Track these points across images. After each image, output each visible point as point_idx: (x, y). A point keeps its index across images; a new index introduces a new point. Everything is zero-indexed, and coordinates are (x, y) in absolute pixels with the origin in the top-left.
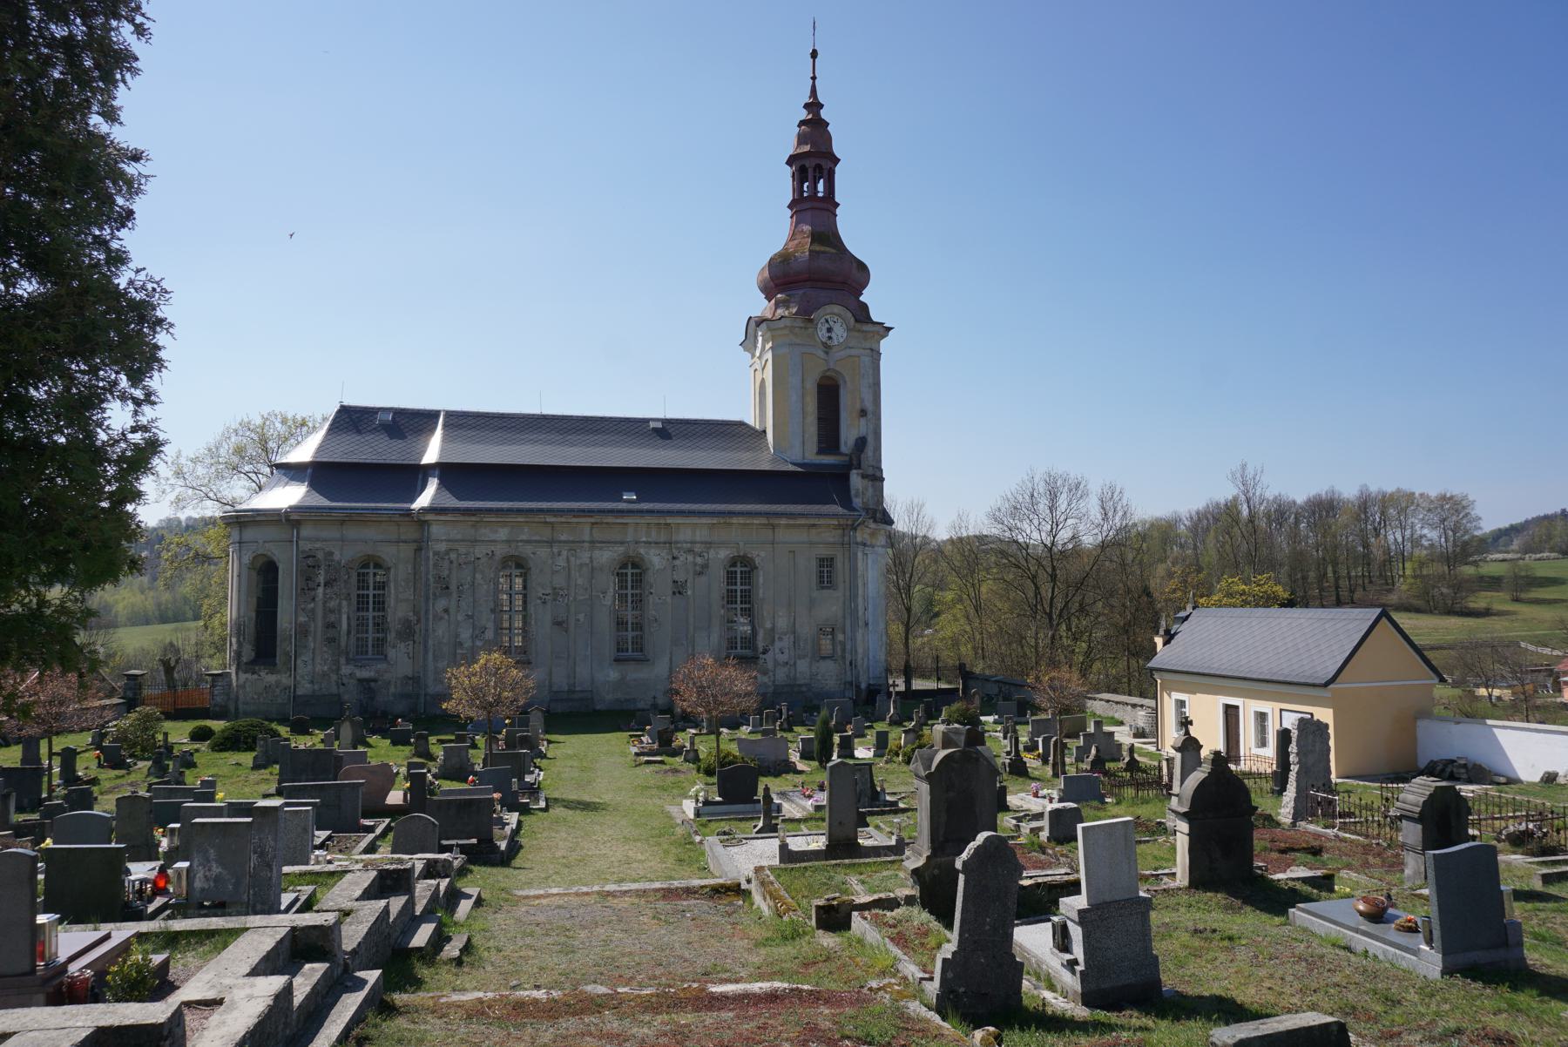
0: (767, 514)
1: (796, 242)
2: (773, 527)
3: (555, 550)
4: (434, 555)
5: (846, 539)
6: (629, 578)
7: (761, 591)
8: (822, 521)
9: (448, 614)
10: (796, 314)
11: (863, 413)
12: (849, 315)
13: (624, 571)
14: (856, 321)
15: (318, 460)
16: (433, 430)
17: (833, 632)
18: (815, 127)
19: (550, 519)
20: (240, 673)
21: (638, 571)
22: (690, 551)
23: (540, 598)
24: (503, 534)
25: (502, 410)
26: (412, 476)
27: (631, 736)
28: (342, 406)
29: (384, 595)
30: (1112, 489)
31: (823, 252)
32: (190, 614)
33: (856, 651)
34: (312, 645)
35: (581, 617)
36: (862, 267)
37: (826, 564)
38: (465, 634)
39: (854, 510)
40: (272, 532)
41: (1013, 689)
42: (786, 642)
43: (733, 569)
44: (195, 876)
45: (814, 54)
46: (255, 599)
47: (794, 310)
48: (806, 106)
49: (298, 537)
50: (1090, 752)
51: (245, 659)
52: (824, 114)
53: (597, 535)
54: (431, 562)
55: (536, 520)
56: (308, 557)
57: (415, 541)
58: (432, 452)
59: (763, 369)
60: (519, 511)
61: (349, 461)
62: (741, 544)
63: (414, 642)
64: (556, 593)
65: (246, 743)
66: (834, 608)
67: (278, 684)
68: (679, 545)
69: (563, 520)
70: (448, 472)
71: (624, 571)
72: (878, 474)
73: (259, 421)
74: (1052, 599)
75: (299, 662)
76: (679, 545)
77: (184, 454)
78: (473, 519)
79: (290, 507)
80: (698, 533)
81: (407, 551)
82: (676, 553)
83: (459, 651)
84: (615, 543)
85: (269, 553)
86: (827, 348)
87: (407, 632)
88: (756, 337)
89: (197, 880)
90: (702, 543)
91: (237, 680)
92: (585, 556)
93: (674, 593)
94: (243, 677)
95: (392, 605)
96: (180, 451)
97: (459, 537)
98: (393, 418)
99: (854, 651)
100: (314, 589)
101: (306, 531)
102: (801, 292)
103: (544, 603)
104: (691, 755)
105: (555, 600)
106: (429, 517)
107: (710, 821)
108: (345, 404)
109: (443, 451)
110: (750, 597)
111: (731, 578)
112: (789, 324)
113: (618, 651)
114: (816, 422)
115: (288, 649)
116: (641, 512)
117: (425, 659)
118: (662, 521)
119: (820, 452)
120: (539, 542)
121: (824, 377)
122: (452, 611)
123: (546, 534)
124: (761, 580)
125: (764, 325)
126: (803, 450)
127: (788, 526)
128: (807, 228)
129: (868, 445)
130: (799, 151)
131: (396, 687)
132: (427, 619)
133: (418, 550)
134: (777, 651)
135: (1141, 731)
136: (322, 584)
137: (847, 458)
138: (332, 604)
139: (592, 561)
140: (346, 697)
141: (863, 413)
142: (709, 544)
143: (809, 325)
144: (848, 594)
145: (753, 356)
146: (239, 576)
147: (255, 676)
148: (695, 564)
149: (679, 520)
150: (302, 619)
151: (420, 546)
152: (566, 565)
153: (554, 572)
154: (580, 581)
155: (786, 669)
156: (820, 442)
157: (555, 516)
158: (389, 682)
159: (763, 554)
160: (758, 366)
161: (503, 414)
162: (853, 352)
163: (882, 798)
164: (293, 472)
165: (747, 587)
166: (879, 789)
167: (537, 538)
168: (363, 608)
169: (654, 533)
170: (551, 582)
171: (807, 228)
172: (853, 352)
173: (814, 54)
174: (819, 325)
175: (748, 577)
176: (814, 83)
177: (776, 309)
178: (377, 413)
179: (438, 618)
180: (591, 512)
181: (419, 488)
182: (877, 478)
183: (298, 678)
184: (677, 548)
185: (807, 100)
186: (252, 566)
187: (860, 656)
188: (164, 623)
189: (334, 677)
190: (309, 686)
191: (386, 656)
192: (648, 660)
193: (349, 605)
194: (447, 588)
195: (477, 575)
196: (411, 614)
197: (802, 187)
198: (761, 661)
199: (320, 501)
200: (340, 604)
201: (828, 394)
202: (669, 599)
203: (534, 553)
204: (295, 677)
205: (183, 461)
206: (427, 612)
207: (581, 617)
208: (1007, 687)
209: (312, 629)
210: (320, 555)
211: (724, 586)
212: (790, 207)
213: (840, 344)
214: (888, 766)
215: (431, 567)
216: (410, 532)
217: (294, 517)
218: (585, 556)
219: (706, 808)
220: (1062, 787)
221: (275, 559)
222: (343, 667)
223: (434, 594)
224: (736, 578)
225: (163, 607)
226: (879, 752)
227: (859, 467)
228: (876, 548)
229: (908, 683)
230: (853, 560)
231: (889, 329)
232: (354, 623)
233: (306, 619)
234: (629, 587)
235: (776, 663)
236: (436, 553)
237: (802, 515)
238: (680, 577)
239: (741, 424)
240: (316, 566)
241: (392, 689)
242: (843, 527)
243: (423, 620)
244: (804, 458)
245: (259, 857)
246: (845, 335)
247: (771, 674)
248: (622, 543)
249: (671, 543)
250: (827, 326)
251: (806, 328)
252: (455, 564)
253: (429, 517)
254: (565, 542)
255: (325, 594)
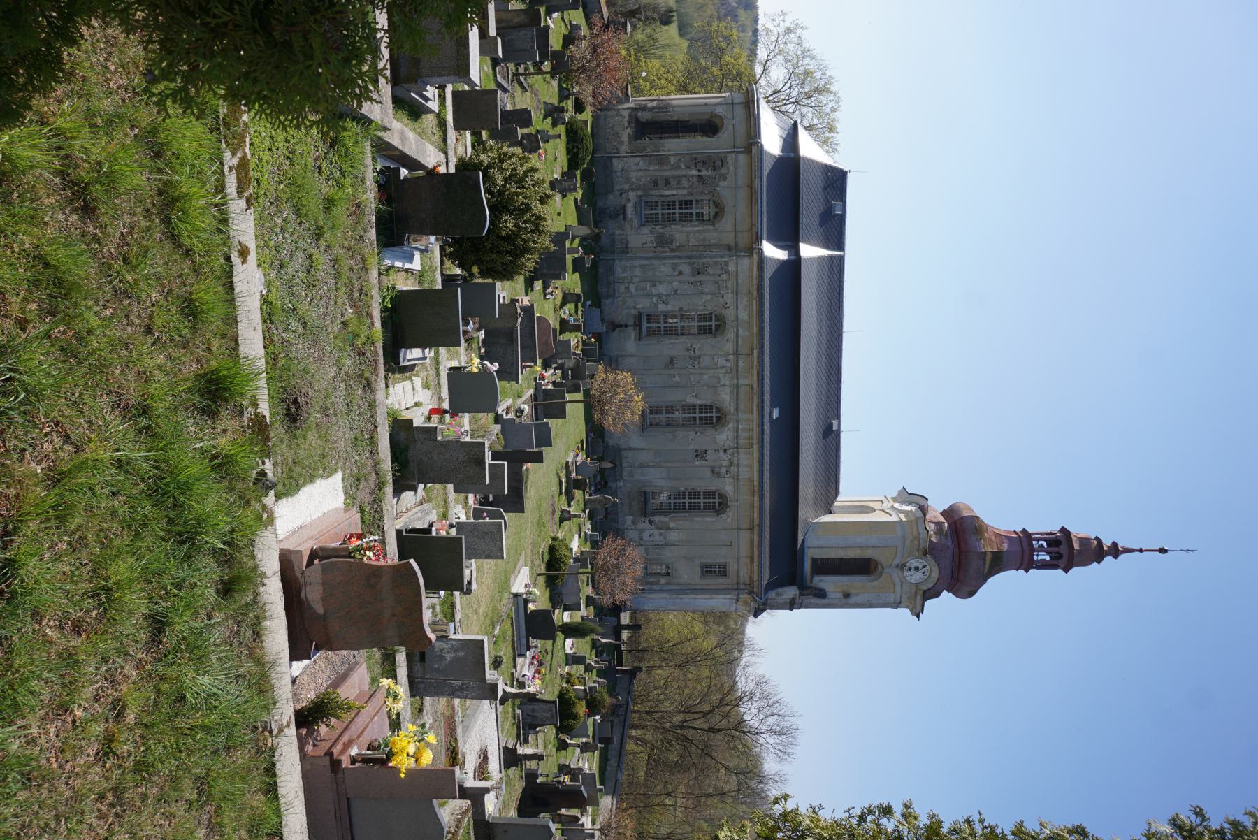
0: (761, 525)
1: (993, 538)
2: (751, 529)
4: (725, 262)
5: (742, 586)
7: (699, 519)
8: (756, 568)
9: (678, 275)
10: (931, 541)
11: (847, 596)
14: (925, 591)
15: (801, 161)
16: (827, 247)
17: (668, 574)
18: (1095, 552)
19: (756, 353)
20: (629, 111)
21: (714, 421)
22: (731, 463)
23: (691, 347)
24: (743, 315)
26: (789, 237)
29: (692, 220)
34: (652, 168)
35: (677, 379)
36: (972, 593)
37: (722, 571)
38: (662, 289)
39: (766, 592)
40: (741, 130)
42: (658, 539)
45: (1163, 551)
46: (688, 119)
47: (934, 539)
48: (1115, 545)
49: (738, 152)
53: (742, 390)
54: (719, 259)
55: (755, 342)
56: (722, 161)
57: (736, 245)
58: (808, 251)
59: (883, 511)
60: (762, 329)
61: (801, 186)
62: (737, 504)
63: (655, 247)
64: (696, 358)
65: (573, 148)
66: (686, 576)
67: (621, 143)
68: (736, 455)
69: (755, 363)
70: (793, 266)
72: (796, 606)
73: (833, 89)
74: (695, 729)
75: (638, 159)
76: (736, 455)
78: (755, 292)
79: (762, 146)
80: (746, 469)
81: (728, 239)
82: (730, 452)
83: (648, 285)
84: (737, 404)
85: (724, 129)
86: (902, 567)
87: (663, 242)
88: (910, 503)
89: (441, 643)
90: (738, 472)
92: (726, 380)
93: (697, 451)
94: (626, 114)
95: (684, 229)
96: (806, 29)
98: (838, 215)
101: (742, 159)
102: (950, 544)
103: (688, 350)
104: (566, 515)
105: (690, 358)
106: (756, 257)
107: (512, 618)
109: (811, 260)
110: (695, 509)
111: (710, 495)
112: (922, 536)
113: (648, 316)
115: (648, 150)
116: (763, 424)
117: (642, 258)
118: (755, 441)
119: (814, 561)
121: (876, 563)
122: (681, 278)
123: (744, 349)
124: (708, 519)
125: (920, 514)
126: (815, 547)
127: (752, 541)
128: (1005, 547)
129: (819, 598)
130: (1074, 539)
131: (620, 235)
132: (673, 258)
133: (729, 248)
136: (700, 174)
138: (684, 183)
140: (611, 197)
141: (847, 596)
143: (921, 553)
145: (895, 500)
146: (706, 104)
147: (626, 124)
148: (720, 468)
149: (756, 455)
150: (672, 160)
151: (732, 249)
153: (712, 357)
154: (705, 377)
157: (758, 357)
158: (623, 229)
159: (729, 520)
160: (887, 505)
161: (842, 301)
162: (898, 588)
163: (531, 731)
164: (791, 141)
166: (538, 729)
168: (681, 205)
169: (746, 434)
171: (1005, 547)
172: (898, 588)
173: (1163, 551)
174: (921, 561)
175: (709, 508)
176: (1137, 551)
177: (934, 523)
178: (841, 201)
179: (674, 267)
180: (762, 386)
181: (780, 243)
182: (792, 605)
183: (626, 159)
185: (1121, 545)
186: (713, 115)
187: (648, 596)
189: (626, 187)
190: (620, 167)
191: (644, 225)
193: (684, 195)
194: (699, 273)
195: (709, 296)
196: (678, 244)
198: (643, 519)
199: (767, 166)
200: (684, 188)
201: (863, 567)
202: (692, 447)
203: (727, 340)
204: (626, 157)
205: (799, 31)
206: (680, 258)
207: (677, 379)
208: (623, 713)
209: (665, 168)
210: (723, 171)
212: (1024, 531)
214: (558, 677)
216: (743, 240)
217: (754, 149)
218: (726, 380)
222: (635, 193)
223: (694, 263)
224: (709, 498)
227: (801, 594)
228: (734, 605)
229: (627, 627)
230: (725, 591)
231: (918, 616)
234: (701, 415)
235: (642, 531)
236: (726, 263)
237: (761, 553)
238: (710, 456)
239: (837, 493)
241: (617, 232)
243: (673, 254)
244: (808, 548)
246: (912, 581)
247: (633, 527)
248: (737, 409)
249: (737, 448)
250: (920, 567)
251: (918, 550)
252: (718, 278)
253: (756, 257)
254: (737, 365)
255: (692, 176)
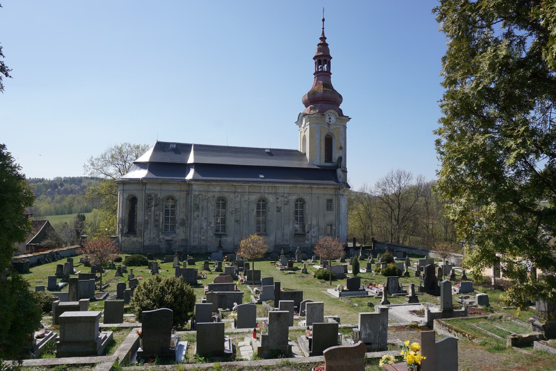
0: (310, 184)
2: (312, 188)
3: (236, 195)
6: (261, 205)
7: (307, 211)
8: (329, 187)
10: (318, 112)
11: (341, 148)
12: (337, 113)
13: (260, 203)
17: (331, 225)
18: (323, 46)
19: (235, 184)
20: (123, 237)
22: (283, 196)
23: (231, 212)
24: (218, 189)
25: (278, 148)
27: (271, 263)
28: (157, 142)
30: (421, 177)
31: (328, 91)
32: (66, 212)
33: (339, 233)
34: (150, 227)
35: (245, 219)
36: (340, 96)
37: (330, 201)
38: (204, 224)
39: (339, 182)
40: (135, 187)
41: (394, 247)
42: (316, 229)
43: (297, 203)
44: (362, 334)
45: (323, 20)
46: (128, 211)
47: (317, 111)
48: (321, 38)
49: (145, 189)
50: (450, 272)
51: (124, 232)
52: (327, 41)
53: (251, 190)
54: (193, 199)
55: (230, 184)
56: (149, 196)
58: (191, 159)
59: (305, 132)
60: (224, 181)
63: (186, 227)
64: (236, 210)
67: (137, 241)
68: (279, 194)
69: (239, 184)
70: (197, 166)
71: (260, 203)
73: (120, 146)
75: (145, 233)
76: (279, 194)
77: (94, 157)
78: (208, 183)
79: (143, 178)
81: (184, 194)
82: (278, 197)
83: (202, 231)
84: (257, 193)
87: (183, 223)
88: (302, 120)
89: (362, 335)
90: (287, 193)
91: (122, 239)
93: (277, 211)
94: (124, 238)
95: (178, 214)
96: (92, 156)
97: (202, 190)
98: (176, 146)
99: (339, 233)
100: (151, 207)
101: (148, 187)
102: (319, 105)
103: (232, 214)
104: (304, 271)
105: (236, 213)
107: (351, 297)
108: (159, 141)
109: (195, 159)
114: (324, 151)
115: (141, 229)
116: (266, 182)
118: (274, 186)
119: (326, 161)
120: (231, 192)
121: (327, 135)
122: (200, 216)
123: (233, 189)
124: (307, 207)
125: (307, 116)
126: (320, 161)
128: (321, 82)
129: (342, 160)
130: (318, 54)
131: (179, 243)
134: (312, 232)
135: (453, 264)
136: (154, 206)
137: (336, 164)
138: (157, 213)
139: (249, 199)
140: (161, 246)
141: (341, 148)
142: (289, 194)
144: (337, 212)
145: (300, 127)
146: (123, 202)
147: (129, 238)
148: (285, 201)
149: (279, 185)
150: (146, 218)
151: (188, 193)
152: (240, 200)
153: (236, 203)
154: (245, 206)
155: (315, 239)
156: (325, 158)
157: (236, 183)
158: (177, 241)
159: (308, 198)
160: (302, 130)
161: (214, 146)
162: (338, 126)
163: (401, 289)
164: (142, 165)
165: (302, 209)
166: (400, 286)
167: (230, 191)
169: (270, 190)
170: (234, 206)
171: (321, 82)
172: (338, 126)
173: (323, 20)
174: (326, 117)
175: (302, 206)
176: (323, 30)
177: (310, 110)
179: (195, 219)
180: (249, 182)
181: (187, 172)
184: (278, 195)
186: (127, 199)
187: (341, 234)
188: (57, 215)
189: (157, 239)
190: (148, 242)
191: (175, 232)
192: (268, 235)
193: (163, 213)
194: (198, 208)
196: (185, 217)
197: (318, 67)
201: (329, 141)
202: (275, 213)
204: (144, 239)
205: (93, 160)
206: (191, 216)
207: (245, 219)
208: (392, 246)
210: (153, 195)
211: (294, 209)
212: (314, 74)
213: (333, 124)
214: (377, 276)
215: (193, 200)
216: (184, 188)
217: (144, 181)
219: (343, 292)
220: (460, 286)
221: (136, 196)
222: (161, 236)
223: (194, 210)
225: (57, 209)
226: (368, 270)
227: (340, 168)
228: (345, 196)
229: (354, 244)
231: (350, 118)
232: (164, 219)
233: (148, 218)
235: (312, 237)
236: (195, 195)
238: (279, 205)
239: (297, 151)
240: (151, 199)
241: (177, 244)
242: (335, 189)
243: (189, 219)
245: (382, 326)
247: (310, 240)
248: (259, 193)
249: (276, 193)
250: (329, 117)
254: (240, 192)
255: (154, 209)
